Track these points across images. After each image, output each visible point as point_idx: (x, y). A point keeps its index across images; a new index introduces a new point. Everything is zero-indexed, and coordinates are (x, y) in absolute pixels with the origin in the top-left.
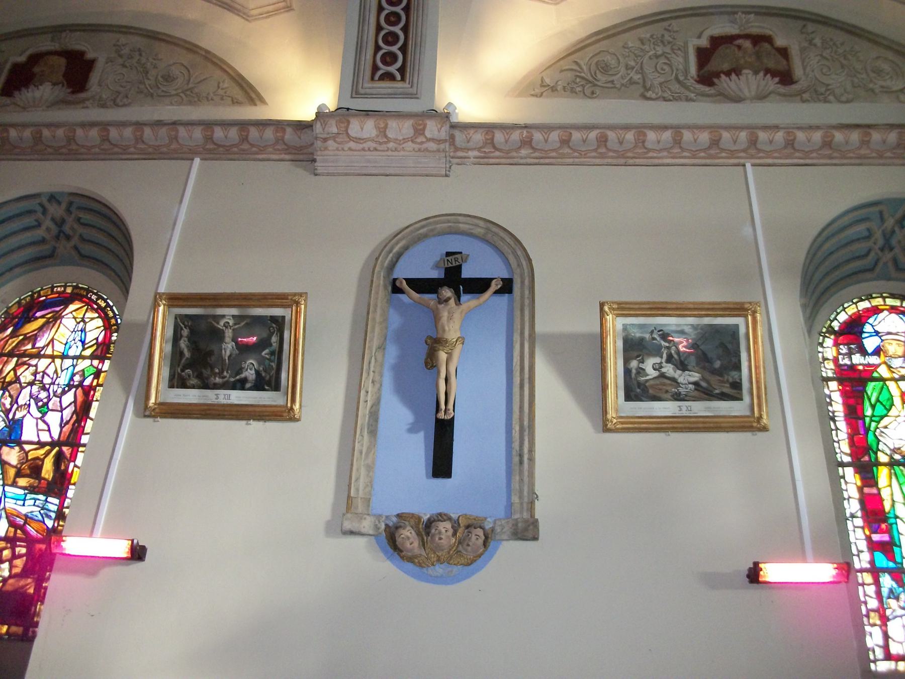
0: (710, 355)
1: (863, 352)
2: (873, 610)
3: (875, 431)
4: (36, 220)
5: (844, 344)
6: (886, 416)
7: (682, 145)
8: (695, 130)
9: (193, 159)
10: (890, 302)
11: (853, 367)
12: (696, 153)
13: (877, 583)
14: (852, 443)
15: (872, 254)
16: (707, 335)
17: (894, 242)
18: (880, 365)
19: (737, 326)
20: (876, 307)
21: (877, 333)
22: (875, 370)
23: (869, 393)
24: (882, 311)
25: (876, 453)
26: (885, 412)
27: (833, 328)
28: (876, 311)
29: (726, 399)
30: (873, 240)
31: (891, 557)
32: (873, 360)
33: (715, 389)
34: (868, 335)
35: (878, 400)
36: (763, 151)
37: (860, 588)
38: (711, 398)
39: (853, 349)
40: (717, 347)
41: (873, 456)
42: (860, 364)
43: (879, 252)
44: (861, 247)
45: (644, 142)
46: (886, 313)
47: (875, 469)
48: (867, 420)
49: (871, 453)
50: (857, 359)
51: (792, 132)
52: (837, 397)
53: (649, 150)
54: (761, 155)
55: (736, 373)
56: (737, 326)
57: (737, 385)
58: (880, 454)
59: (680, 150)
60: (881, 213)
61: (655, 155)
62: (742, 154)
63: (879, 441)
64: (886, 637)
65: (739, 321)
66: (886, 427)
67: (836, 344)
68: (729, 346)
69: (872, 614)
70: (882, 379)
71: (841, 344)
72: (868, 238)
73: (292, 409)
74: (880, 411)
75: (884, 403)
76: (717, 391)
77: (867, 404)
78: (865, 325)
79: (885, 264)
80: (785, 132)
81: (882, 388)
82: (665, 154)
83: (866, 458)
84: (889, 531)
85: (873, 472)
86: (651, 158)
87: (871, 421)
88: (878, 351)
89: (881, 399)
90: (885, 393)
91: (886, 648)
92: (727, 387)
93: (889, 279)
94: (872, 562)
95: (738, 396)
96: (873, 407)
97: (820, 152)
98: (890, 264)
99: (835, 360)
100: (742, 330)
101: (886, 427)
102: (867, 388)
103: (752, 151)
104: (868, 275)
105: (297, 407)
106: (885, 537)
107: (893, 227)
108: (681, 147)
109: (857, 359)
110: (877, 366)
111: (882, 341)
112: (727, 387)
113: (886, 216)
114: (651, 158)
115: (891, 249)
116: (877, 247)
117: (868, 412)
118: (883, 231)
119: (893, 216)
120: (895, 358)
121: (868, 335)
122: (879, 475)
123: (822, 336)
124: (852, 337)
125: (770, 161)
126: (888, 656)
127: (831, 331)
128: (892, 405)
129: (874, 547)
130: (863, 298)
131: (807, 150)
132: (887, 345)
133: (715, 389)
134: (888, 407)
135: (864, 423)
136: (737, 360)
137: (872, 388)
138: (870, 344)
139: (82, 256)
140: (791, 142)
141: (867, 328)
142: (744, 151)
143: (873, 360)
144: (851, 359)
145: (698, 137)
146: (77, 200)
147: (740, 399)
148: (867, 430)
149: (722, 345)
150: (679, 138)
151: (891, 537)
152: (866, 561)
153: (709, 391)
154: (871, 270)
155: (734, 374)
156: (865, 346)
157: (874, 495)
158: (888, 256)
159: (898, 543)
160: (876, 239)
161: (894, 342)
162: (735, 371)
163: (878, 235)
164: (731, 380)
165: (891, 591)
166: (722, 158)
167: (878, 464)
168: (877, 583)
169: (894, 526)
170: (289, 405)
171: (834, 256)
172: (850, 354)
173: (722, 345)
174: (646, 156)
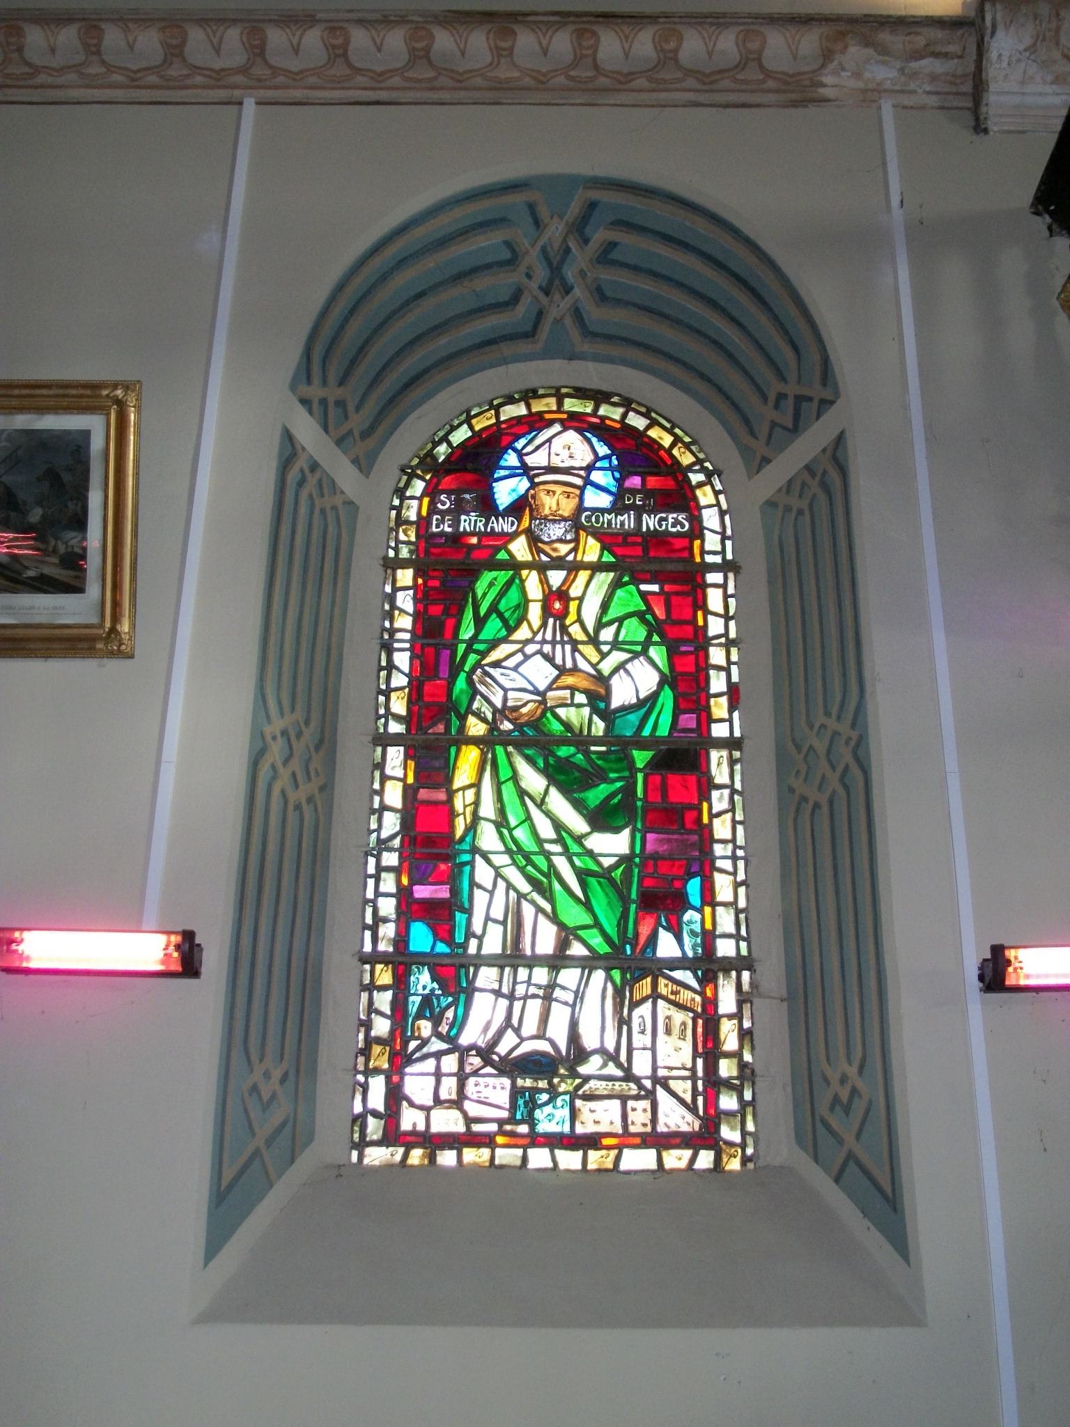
0: (22, 496)
1: (487, 506)
2: (379, 1041)
3: (473, 670)
4: (508, 244)
5: (449, 493)
6: (505, 640)
7: (105, 57)
8: (131, 25)
9: (241, 103)
10: (571, 405)
11: (457, 538)
12: (139, 75)
13: (401, 985)
14: (416, 690)
15: (526, 301)
16: (20, 452)
17: (570, 274)
18: (515, 535)
19: (86, 434)
20: (540, 414)
21: (525, 470)
22: (504, 547)
23: (479, 593)
24: (550, 423)
25: (463, 719)
26: (504, 633)
27: (435, 458)
28: (536, 423)
29: (51, 590)
30: (522, 269)
31: (443, 931)
32: (503, 525)
33: (27, 568)
34: (507, 472)
35: (494, 608)
36: (286, 72)
37: (364, 996)
38: (18, 586)
39: (468, 502)
40: (39, 480)
41: (455, 723)
42: (473, 534)
43: (541, 296)
44: (497, 284)
45: (20, 49)
46: (557, 428)
47: (453, 750)
48: (461, 648)
49: (454, 718)
50: (469, 522)
51: (341, 28)
52: (405, 601)
53: (37, 70)
54: (281, 79)
55: (73, 534)
56: (86, 434)
57: (75, 561)
58: (471, 720)
59: (103, 70)
60: (531, 207)
61: (50, 80)
62: (239, 79)
63: (475, 692)
64: (395, 1096)
65: (94, 425)
66: (497, 664)
67: (431, 492)
68: (66, 477)
69: (377, 1049)
70: (515, 566)
71: (443, 492)
72: (512, 261)
73: (113, 630)
74: (493, 627)
75: (507, 615)
76: (31, 573)
77: (468, 615)
78: (506, 452)
79: (558, 321)
80: (326, 29)
81: (509, 584)
82: (71, 77)
83: (441, 728)
84: (452, 879)
85: (448, 759)
86: (42, 86)
87: (469, 649)
88: (519, 507)
89: (502, 606)
90: (513, 596)
91: (391, 1115)
92: (54, 564)
93: (572, 357)
94: (401, 940)
95: (76, 583)
96: (480, 622)
97: (410, 74)
98: (568, 321)
99: (422, 524)
100: (97, 444)
101: (497, 664)
102: (478, 584)
103: (259, 71)
104: (523, 347)
105: (125, 627)
106: (443, 892)
107: (564, 240)
108: (103, 62)
109: (469, 522)
110: (512, 537)
111: (533, 485)
112: (54, 564)
113: (543, 212)
114: (42, 86)
115: (568, 290)
116: (534, 285)
117: (467, 632)
118: (544, 250)
119: (561, 217)
120: (554, 521)
121: (507, 472)
122: (459, 764)
123: (406, 473)
124: (469, 477)
125: (298, 94)
126: (392, 1136)
127: (428, 461)
128: (523, 618)
129: (409, 908)
130: (516, 396)
131: (379, 69)
132: (542, 495)
133: (27, 568)
134: (512, 623)
135: (454, 652)
136: (79, 509)
137: (487, 584)
138: (506, 491)
139: (590, 334)
140: (340, 51)
141: (511, 459)
142: (244, 70)
143: (503, 525)
144: (457, 522)
145: (135, 40)
146: (606, 197)
147: (80, 590)
148: (455, 670)
149: (52, 476)
150: (95, 41)
151: (455, 892)
152: (389, 940)
153: (14, 571)
154: (530, 334)
155: (71, 536)
156: (496, 496)
157: (436, 803)
158: (559, 307)
159: (466, 905)
160: (529, 267)
161: (559, 489)
162: (75, 530)
163: (533, 257)
164: (62, 549)
165: (427, 1001)
166: (196, 87)
167: (463, 739)
168: (401, 985)
169: (467, 869)
170: (108, 624)
171: (429, 303)
172: (459, 509)
173: (52, 476)
174: (31, 82)
